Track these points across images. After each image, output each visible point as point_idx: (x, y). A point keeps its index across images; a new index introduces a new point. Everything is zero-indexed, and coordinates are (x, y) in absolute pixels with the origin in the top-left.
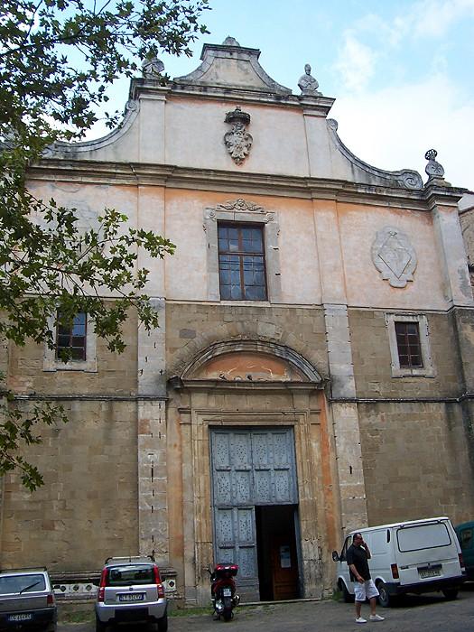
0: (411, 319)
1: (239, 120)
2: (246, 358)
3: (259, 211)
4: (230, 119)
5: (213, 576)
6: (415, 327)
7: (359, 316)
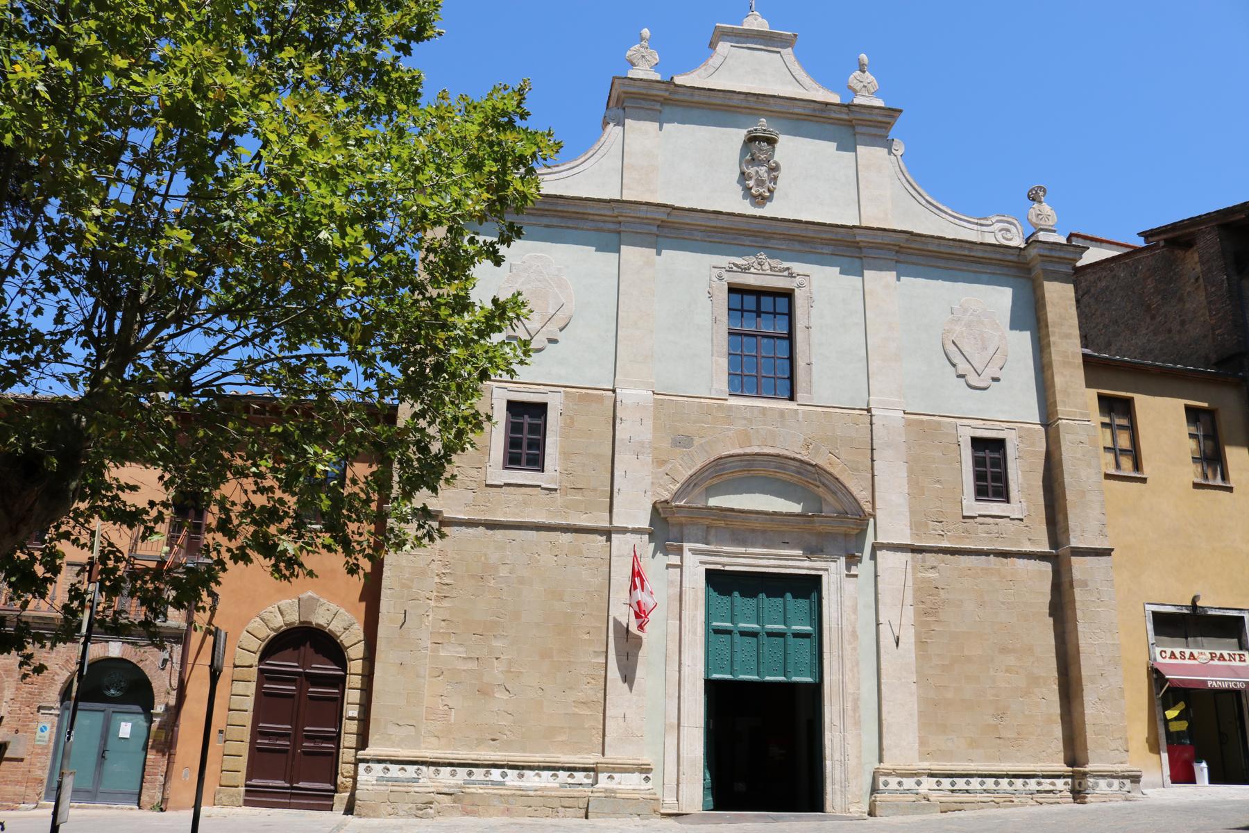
0: (1235, 614)
1: (758, 144)
2: (1083, 714)
3: (786, 273)
4: (751, 140)
5: (88, 288)
6: (782, 303)
7: (923, 429)
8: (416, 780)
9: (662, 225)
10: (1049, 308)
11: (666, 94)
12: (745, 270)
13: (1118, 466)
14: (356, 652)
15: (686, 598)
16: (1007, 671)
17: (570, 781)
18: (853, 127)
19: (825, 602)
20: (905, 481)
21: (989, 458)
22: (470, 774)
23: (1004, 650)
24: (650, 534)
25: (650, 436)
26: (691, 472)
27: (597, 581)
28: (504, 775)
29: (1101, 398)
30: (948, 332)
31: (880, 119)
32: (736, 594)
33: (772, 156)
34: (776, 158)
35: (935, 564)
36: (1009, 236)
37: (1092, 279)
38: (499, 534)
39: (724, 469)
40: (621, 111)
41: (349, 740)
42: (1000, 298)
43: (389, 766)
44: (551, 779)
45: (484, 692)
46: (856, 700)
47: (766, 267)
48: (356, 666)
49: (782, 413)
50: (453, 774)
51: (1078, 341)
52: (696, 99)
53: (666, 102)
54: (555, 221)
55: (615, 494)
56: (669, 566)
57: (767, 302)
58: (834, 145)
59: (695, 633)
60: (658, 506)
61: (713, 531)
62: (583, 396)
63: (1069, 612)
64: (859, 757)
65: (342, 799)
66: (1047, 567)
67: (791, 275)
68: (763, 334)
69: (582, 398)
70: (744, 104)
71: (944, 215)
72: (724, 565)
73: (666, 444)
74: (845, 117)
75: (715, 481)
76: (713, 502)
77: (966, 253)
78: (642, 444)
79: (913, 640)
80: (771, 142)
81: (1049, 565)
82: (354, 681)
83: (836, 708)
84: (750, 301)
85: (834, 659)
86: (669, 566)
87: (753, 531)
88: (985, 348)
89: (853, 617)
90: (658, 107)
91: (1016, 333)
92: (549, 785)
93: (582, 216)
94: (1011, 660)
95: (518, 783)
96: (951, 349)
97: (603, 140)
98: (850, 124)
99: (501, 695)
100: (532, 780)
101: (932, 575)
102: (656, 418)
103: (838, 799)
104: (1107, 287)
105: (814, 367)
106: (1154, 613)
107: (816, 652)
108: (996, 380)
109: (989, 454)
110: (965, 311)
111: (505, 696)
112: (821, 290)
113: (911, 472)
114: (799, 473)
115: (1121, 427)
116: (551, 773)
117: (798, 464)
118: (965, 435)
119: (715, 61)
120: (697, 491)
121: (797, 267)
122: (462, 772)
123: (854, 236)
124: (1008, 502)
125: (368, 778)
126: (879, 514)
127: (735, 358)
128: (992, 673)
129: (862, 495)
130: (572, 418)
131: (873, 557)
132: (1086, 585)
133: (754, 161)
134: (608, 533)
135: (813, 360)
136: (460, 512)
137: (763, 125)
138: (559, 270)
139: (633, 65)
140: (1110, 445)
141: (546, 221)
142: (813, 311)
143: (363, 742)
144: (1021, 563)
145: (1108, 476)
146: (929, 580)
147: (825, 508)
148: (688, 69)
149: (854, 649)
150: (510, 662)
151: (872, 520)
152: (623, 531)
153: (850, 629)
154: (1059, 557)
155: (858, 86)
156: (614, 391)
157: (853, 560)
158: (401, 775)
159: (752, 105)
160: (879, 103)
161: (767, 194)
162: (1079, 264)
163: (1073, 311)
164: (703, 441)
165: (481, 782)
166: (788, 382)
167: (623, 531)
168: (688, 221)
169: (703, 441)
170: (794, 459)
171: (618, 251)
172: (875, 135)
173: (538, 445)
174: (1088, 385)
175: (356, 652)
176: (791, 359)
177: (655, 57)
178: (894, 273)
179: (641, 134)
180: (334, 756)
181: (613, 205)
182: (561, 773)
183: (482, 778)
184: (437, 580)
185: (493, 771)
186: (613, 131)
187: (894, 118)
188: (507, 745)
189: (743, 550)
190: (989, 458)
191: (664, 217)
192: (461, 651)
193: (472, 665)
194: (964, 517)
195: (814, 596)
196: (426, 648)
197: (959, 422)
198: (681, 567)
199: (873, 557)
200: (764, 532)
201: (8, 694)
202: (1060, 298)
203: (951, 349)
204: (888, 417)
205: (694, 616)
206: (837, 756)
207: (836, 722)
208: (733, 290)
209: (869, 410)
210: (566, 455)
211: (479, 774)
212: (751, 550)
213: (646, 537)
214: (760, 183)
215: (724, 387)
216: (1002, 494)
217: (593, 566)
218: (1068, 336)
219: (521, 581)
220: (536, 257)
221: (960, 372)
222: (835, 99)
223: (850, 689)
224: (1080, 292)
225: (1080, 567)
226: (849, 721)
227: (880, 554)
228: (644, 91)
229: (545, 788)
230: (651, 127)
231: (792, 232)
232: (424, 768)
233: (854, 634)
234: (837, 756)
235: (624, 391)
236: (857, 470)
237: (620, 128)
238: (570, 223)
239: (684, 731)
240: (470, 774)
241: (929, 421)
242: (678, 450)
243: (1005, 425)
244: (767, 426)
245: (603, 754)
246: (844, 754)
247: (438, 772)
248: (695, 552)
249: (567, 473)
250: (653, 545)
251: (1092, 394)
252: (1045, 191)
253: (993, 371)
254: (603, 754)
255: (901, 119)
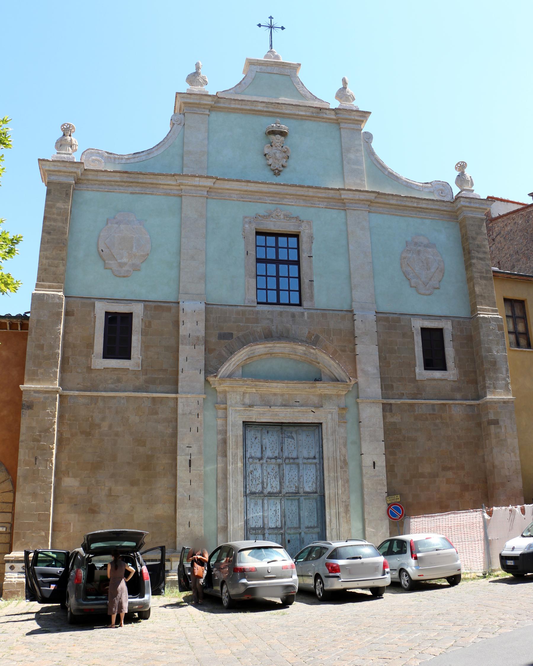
6: (293, 241)
7: (390, 324)
21: (433, 340)
23: (445, 469)
31: (357, 118)
37: (501, 225)
54: (137, 190)
63: (392, 591)
69: (157, 308)
70: (265, 109)
77: (415, 205)
78: (198, 338)
83: (333, 511)
88: (428, 269)
104: (511, 230)
105: (315, 283)
106: (423, 330)
113: (380, 351)
123: (340, 195)
135: (314, 279)
190: (433, 340)
191: (211, 184)
242: (222, 341)
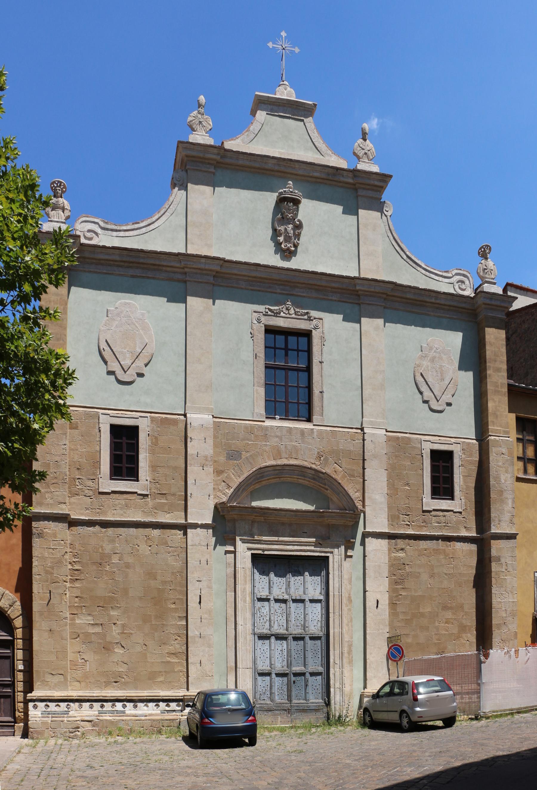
3: (306, 317)
4: (281, 200)
6: (303, 340)
7: (400, 446)
8: (67, 713)
9: (217, 275)
10: (488, 347)
11: (218, 158)
12: (276, 314)
13: (525, 471)
14: (18, 623)
15: (239, 576)
16: (446, 623)
17: (167, 708)
18: (356, 190)
19: (331, 576)
20: (385, 484)
21: (442, 460)
22: (102, 706)
23: (445, 608)
24: (213, 528)
25: (211, 452)
26: (240, 480)
27: (178, 564)
28: (124, 706)
29: (518, 419)
30: (419, 366)
32: (272, 575)
33: (296, 215)
34: (300, 217)
35: (403, 547)
36: (463, 287)
38: (110, 531)
39: (262, 477)
40: (184, 173)
41: (20, 686)
42: (453, 340)
43: (49, 704)
44: (155, 708)
45: (107, 648)
46: (350, 646)
47: (292, 311)
48: (19, 633)
49: (302, 432)
50: (91, 707)
51: (505, 374)
52: (241, 162)
53: (218, 165)
54: (138, 272)
55: (189, 498)
56: (227, 552)
57: (292, 340)
58: (340, 209)
59: (245, 601)
60: (219, 506)
61: (256, 525)
62: (164, 421)
64: (351, 685)
65: (20, 727)
66: (474, 547)
67: (310, 319)
68: (289, 374)
69: (164, 421)
70: (277, 168)
71: (419, 269)
72: (264, 550)
73: (222, 459)
74: (350, 181)
75: (257, 486)
76: (254, 504)
79: (387, 602)
80: (296, 202)
81: (476, 545)
82: (19, 643)
83: (337, 652)
84: (281, 339)
85: (337, 617)
86: (227, 552)
87: (283, 524)
88: (443, 379)
89: (349, 587)
90: (212, 170)
91: (462, 373)
92: (154, 712)
93: (157, 268)
94: (449, 615)
95: (134, 712)
96: (420, 379)
97: (171, 199)
98: (354, 188)
99: (119, 650)
100: (143, 709)
101: (401, 554)
102: (215, 437)
103: (338, 698)
105: (325, 395)
107: (324, 654)
108: (449, 404)
109: (442, 464)
110: (431, 349)
111: (121, 651)
112: (331, 331)
113: (389, 477)
114: (314, 479)
115: (530, 441)
116: (155, 704)
117: (313, 472)
118: (427, 448)
119: (255, 127)
120: (245, 494)
121: (314, 313)
122: (97, 705)
123: (355, 285)
124: (453, 499)
125: (36, 714)
126: (368, 510)
127: (270, 387)
128: (437, 624)
129: (355, 495)
130: (156, 438)
131: (363, 543)
132: (499, 560)
133: (284, 220)
134: (184, 528)
135: (325, 389)
136: (82, 514)
137: (290, 188)
138: (143, 314)
139: (193, 130)
140: (521, 455)
141: (131, 272)
142: (325, 348)
143: (29, 687)
144: (459, 545)
145: (519, 479)
146: (399, 559)
147: (331, 506)
148: (233, 136)
149: (349, 610)
150: (123, 626)
151: (362, 514)
152: (195, 526)
153: (347, 595)
154: (483, 542)
155: (361, 153)
156: (185, 415)
157: (350, 546)
158: (57, 709)
159: (282, 169)
160: (375, 169)
161: (293, 249)
162: (511, 309)
163: (504, 350)
164: (248, 455)
165: (112, 712)
166: (307, 390)
167: (195, 526)
168: (235, 272)
169: (248, 455)
170: (311, 468)
171: (185, 302)
172: (372, 198)
173: (134, 459)
174: (510, 411)
175: (18, 623)
176: (309, 387)
177: (209, 123)
178: (383, 320)
179: (200, 195)
180: (12, 698)
181: (181, 258)
182: (161, 704)
183: (111, 709)
184: (70, 567)
185: (117, 704)
186: (178, 194)
187: (387, 183)
188: (125, 686)
189: (276, 539)
190: (442, 460)
191: (218, 268)
192: (90, 620)
193: (98, 629)
194: (424, 511)
195: (323, 573)
196: (66, 618)
197: (423, 438)
198: (234, 552)
199: (363, 543)
200: (290, 525)
201: (2, 707)
202: (495, 339)
203: (420, 379)
204: (376, 435)
205: (245, 589)
206: (337, 685)
207: (337, 662)
208: (269, 331)
209: (362, 429)
210: (154, 468)
211: (108, 706)
212: (281, 539)
213: (210, 531)
214: (288, 239)
215: (263, 412)
216: (449, 494)
217: (175, 554)
218: (498, 370)
219: (128, 566)
220: (126, 304)
221: (425, 399)
222: (343, 164)
223: (346, 638)
224: (510, 332)
225: (497, 548)
226: (345, 660)
227: (368, 540)
228: (201, 155)
229: (151, 715)
230: (208, 189)
231: (311, 282)
232: (71, 704)
233: (350, 600)
234: (337, 685)
235: (193, 416)
236: (353, 476)
237: (183, 192)
238: (150, 274)
239: (240, 671)
240: (102, 706)
241: (403, 438)
242: (231, 462)
243: (453, 440)
244: (291, 441)
245: (188, 689)
246: (342, 684)
247: (81, 706)
248: (244, 541)
249: (154, 481)
250: (214, 538)
251: (513, 416)
252: (490, 249)
253: (447, 398)
254: (188, 689)
255: (391, 184)
